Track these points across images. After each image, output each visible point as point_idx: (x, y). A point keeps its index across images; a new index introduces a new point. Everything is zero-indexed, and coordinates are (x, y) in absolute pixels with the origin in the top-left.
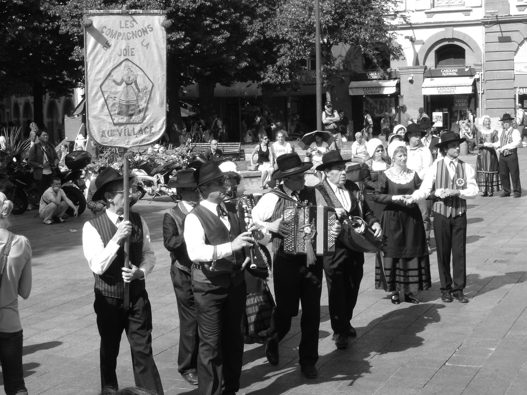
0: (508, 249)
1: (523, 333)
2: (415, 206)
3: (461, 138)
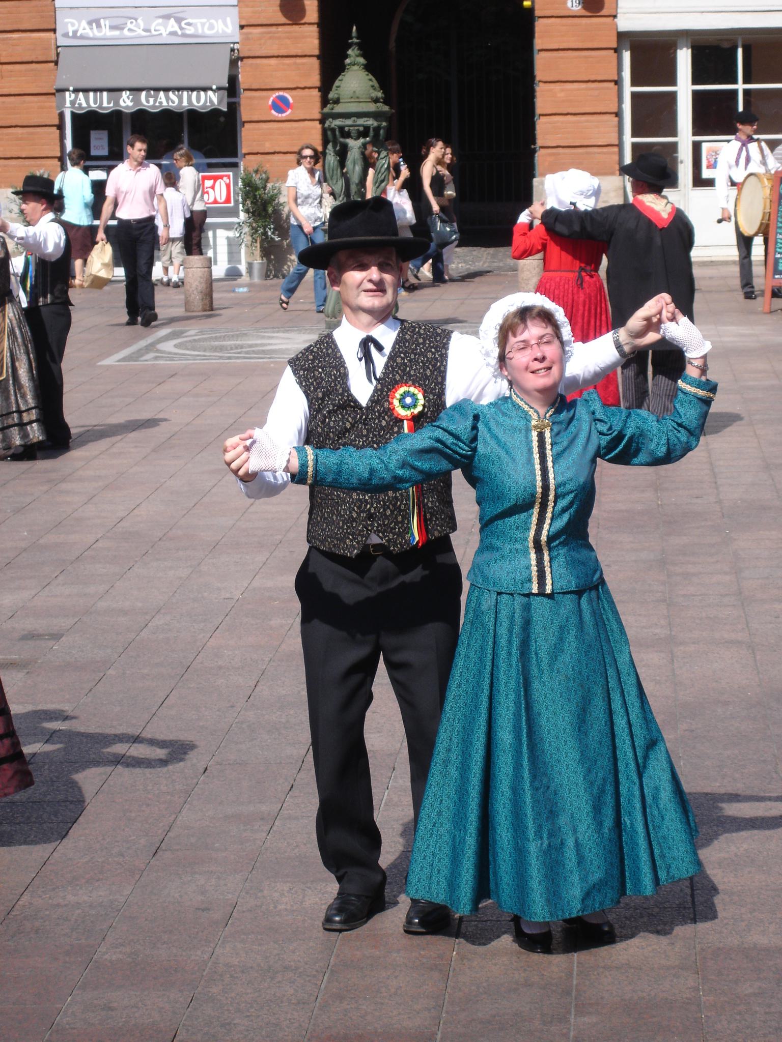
0: (29, 624)
1: (71, 898)
2: (541, 288)
3: (226, 110)
